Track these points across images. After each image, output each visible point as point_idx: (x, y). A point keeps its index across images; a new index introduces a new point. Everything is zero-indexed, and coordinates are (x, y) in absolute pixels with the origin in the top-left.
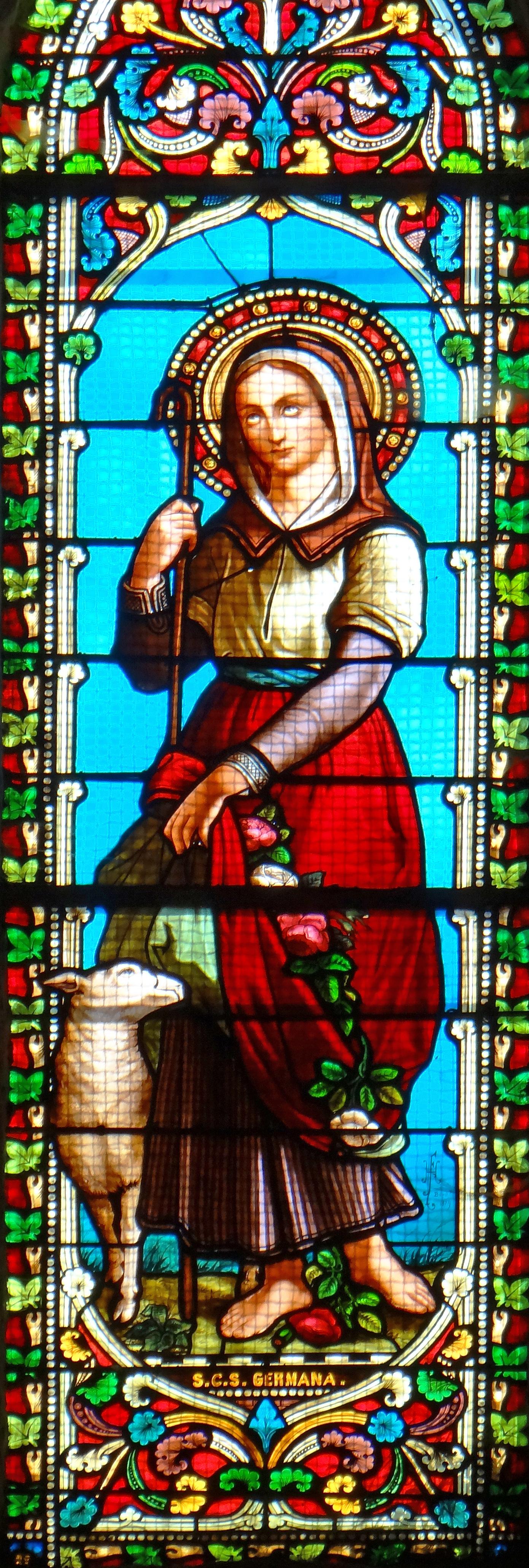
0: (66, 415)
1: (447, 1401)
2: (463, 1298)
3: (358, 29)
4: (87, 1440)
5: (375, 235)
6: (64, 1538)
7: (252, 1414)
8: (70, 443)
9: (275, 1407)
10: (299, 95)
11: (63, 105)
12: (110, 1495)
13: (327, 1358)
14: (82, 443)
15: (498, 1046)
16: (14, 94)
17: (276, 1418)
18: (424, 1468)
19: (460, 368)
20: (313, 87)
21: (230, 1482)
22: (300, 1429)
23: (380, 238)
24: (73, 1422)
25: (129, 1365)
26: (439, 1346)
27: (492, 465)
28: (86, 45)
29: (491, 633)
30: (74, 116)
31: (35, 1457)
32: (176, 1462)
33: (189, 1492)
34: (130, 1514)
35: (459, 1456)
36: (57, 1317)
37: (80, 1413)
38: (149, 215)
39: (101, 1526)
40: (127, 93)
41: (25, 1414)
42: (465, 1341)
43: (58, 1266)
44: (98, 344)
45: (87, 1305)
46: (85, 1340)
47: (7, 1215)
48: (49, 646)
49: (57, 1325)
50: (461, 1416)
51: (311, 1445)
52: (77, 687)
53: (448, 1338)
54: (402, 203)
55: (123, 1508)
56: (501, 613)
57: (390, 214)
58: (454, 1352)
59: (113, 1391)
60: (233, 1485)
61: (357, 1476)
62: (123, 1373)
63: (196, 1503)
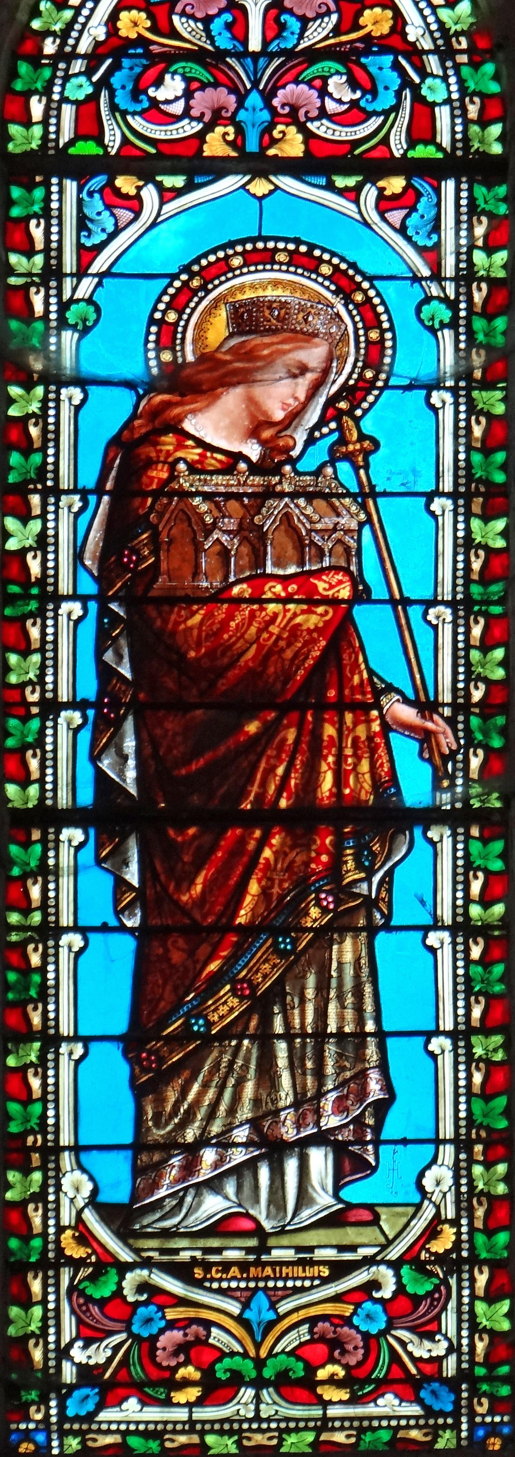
0: (66, 920)
1: (429, 1294)
2: (445, 1194)
3: (337, 31)
4: (88, 1333)
5: (356, 210)
6: (67, 1426)
7: (246, 1305)
8: (69, 614)
9: (269, 1297)
10: (284, 87)
11: (64, 100)
12: (109, 1386)
13: (316, 1251)
14: (82, 944)
15: (473, 558)
16: (15, 212)
17: (268, 1310)
18: (410, 1354)
19: (438, 330)
20: (297, 82)
21: (226, 1371)
22: (295, 1318)
23: (360, 212)
24: (73, 1312)
25: (130, 1260)
26: (422, 1241)
27: (468, 612)
28: (84, 46)
29: (467, 641)
30: (74, 107)
31: (36, 1345)
32: (175, 1354)
33: (186, 1383)
34: (132, 1404)
35: (445, 1344)
36: (57, 1218)
37: (84, 1308)
38: (144, 193)
39: (103, 1416)
40: (123, 87)
41: (27, 1304)
42: (449, 1234)
43: (58, 1169)
44: (98, 310)
45: (86, 1205)
46: (85, 1237)
47: (9, 1334)
48: (50, 589)
49: (57, 1225)
50: (444, 1308)
51: (303, 1333)
52: (78, 408)
53: (432, 1232)
54: (381, 184)
55: (126, 1399)
56: (477, 622)
57: (369, 194)
58: (439, 1246)
59: (114, 1288)
60: (228, 1375)
61: (346, 1367)
62: (123, 1268)
63: (193, 1393)
